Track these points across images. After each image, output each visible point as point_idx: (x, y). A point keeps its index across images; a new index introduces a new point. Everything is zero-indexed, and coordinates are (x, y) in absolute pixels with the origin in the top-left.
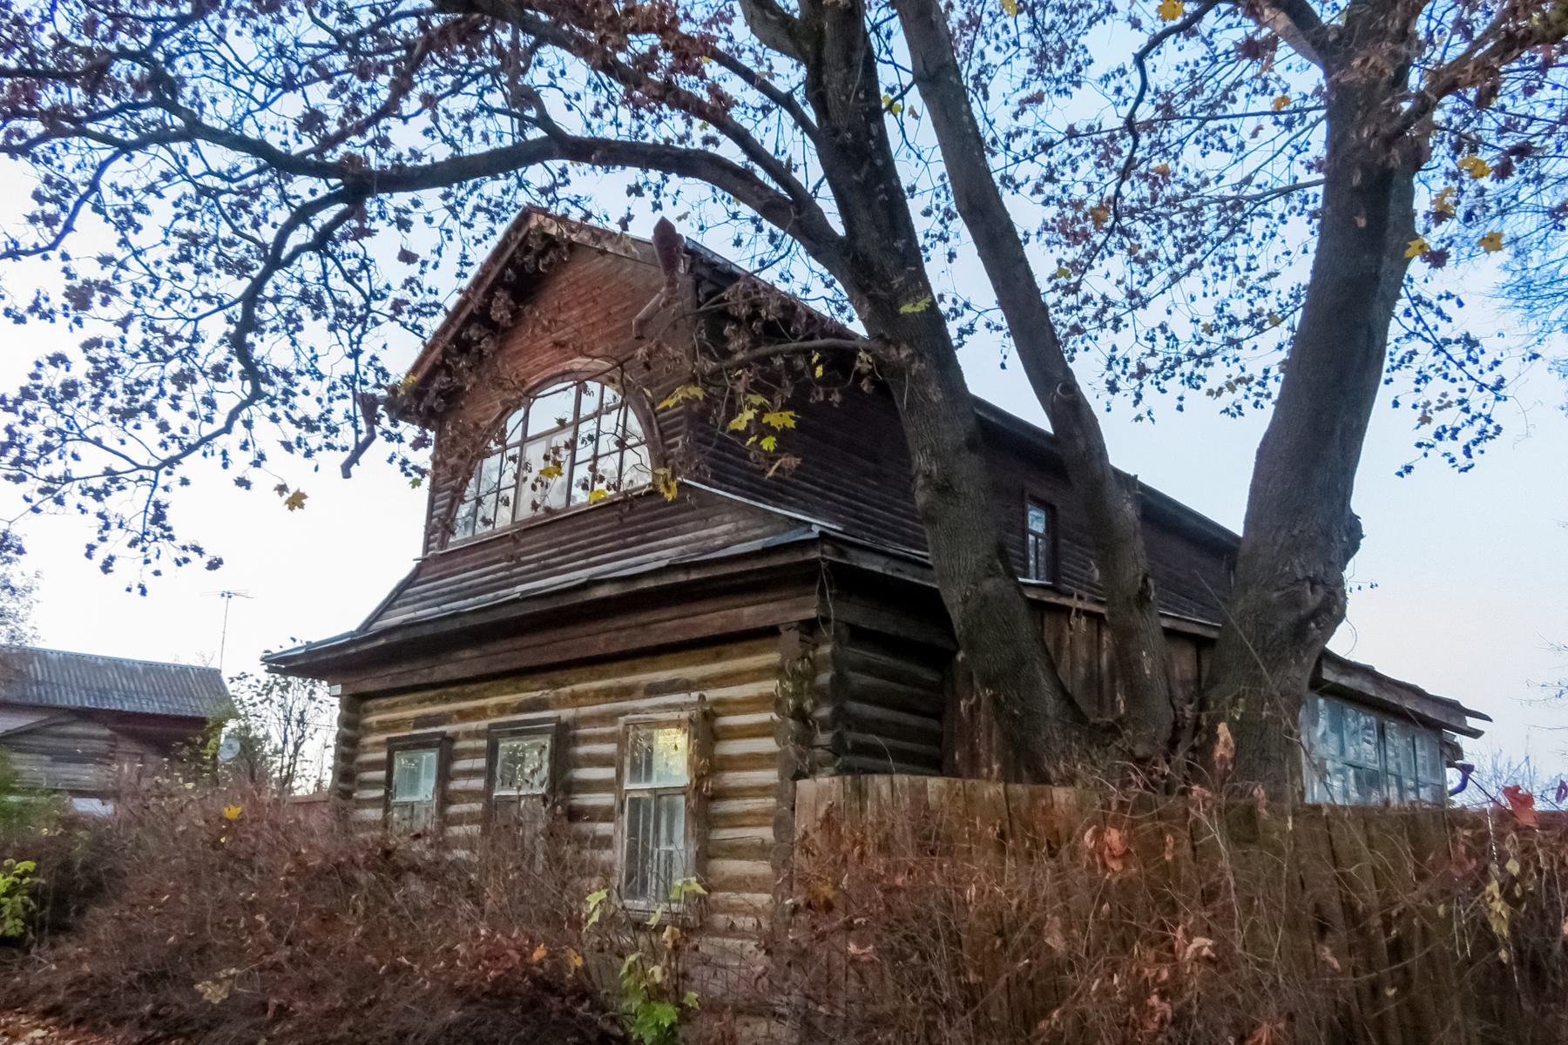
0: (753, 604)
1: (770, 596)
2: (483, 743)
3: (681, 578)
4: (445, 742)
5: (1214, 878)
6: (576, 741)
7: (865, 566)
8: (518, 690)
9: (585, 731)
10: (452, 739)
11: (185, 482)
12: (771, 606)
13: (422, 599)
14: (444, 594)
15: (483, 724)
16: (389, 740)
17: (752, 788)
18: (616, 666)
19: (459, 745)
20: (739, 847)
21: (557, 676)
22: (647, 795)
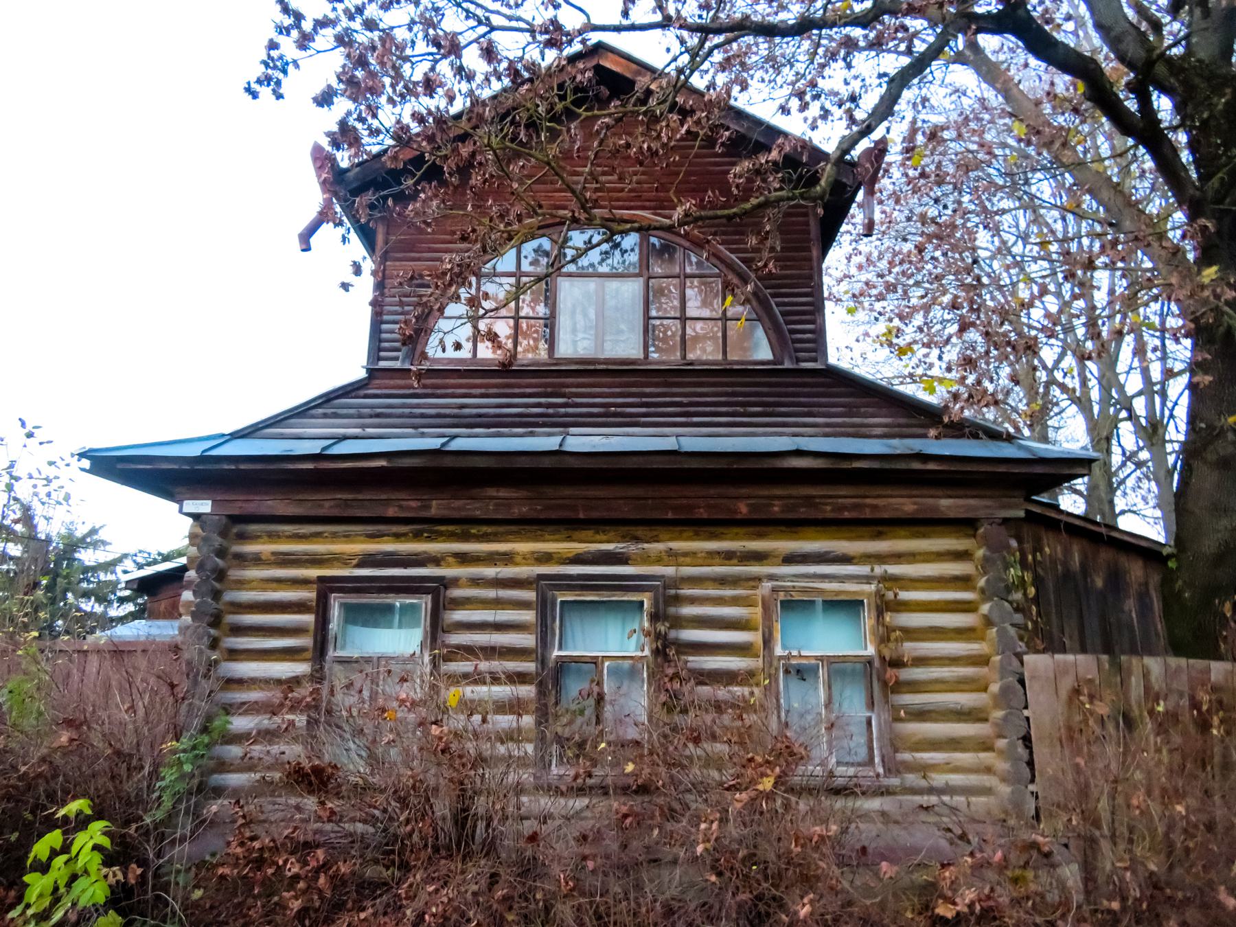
0: (950, 497)
1: (988, 493)
2: (530, 595)
3: (916, 466)
4: (437, 589)
5: (105, 870)
6: (678, 600)
7: (765, 466)
8: (569, 539)
9: (687, 592)
10: (445, 583)
11: (344, 239)
12: (972, 502)
13: (378, 416)
14: (423, 416)
15: (314, 573)
16: (321, 580)
17: (935, 658)
18: (735, 530)
19: (456, 593)
20: (929, 712)
21: (640, 531)
22: (813, 662)
